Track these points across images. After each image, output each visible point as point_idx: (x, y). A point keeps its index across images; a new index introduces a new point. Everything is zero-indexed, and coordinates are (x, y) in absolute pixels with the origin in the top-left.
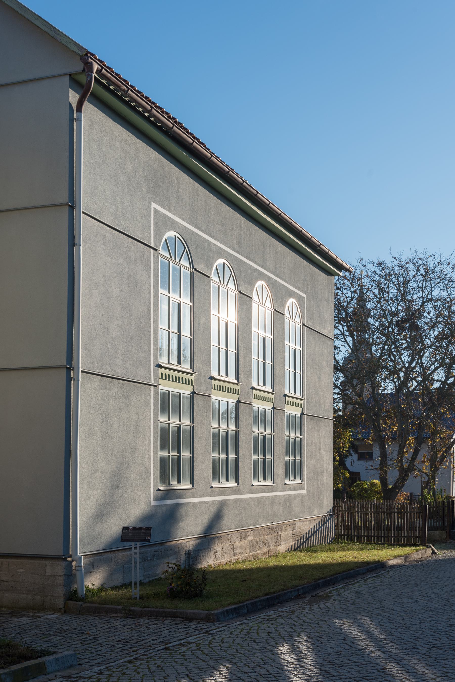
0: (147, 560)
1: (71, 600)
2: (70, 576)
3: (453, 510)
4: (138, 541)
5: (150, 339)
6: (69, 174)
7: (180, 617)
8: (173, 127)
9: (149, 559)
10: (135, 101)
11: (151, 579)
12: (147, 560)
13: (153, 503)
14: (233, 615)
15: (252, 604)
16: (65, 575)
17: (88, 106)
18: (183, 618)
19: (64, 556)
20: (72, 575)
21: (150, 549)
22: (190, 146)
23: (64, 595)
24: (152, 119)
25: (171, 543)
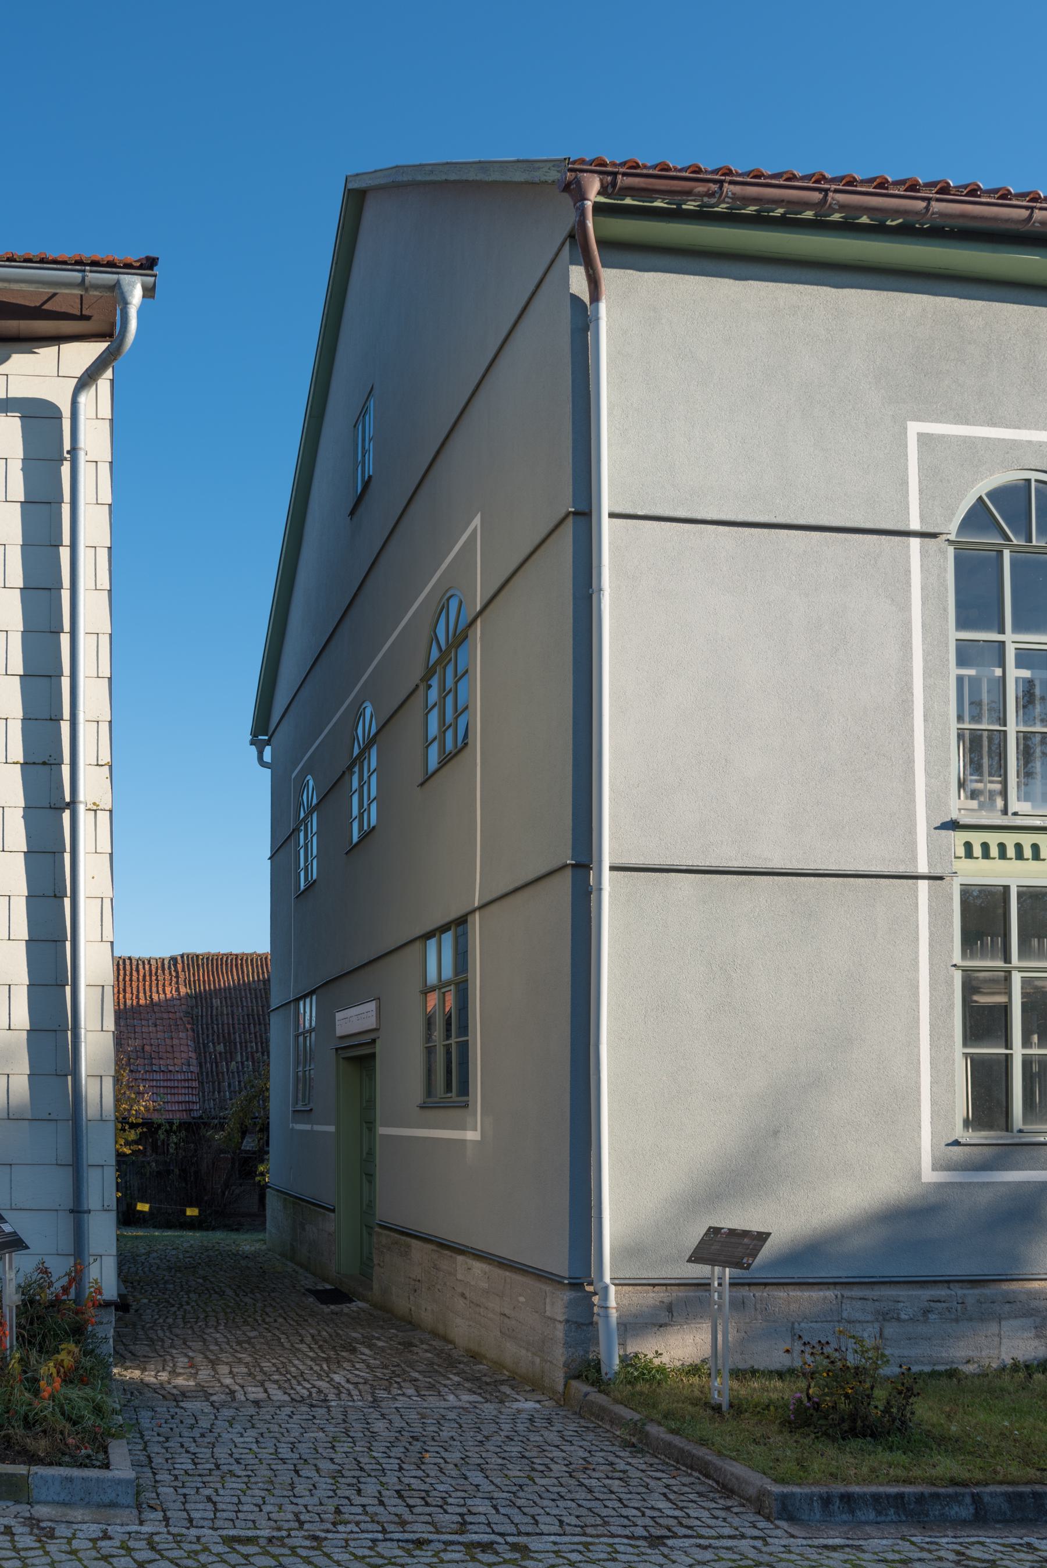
0: (898, 1319)
1: (577, 1377)
2: (584, 1320)
3: (552, 1274)
4: (724, 1264)
5: (910, 761)
6: (574, 441)
7: (714, 1479)
8: (927, 208)
9: (903, 1316)
10: (779, 202)
11: (938, 1368)
12: (898, 1319)
13: (929, 1175)
14: (897, 1513)
15: (1009, 1497)
16: (567, 1321)
17: (608, 276)
18: (717, 1482)
19: (580, 1281)
20: (591, 1323)
21: (910, 1293)
22: (1028, 227)
23: (566, 1365)
24: (864, 220)
25: (1015, 1286)
